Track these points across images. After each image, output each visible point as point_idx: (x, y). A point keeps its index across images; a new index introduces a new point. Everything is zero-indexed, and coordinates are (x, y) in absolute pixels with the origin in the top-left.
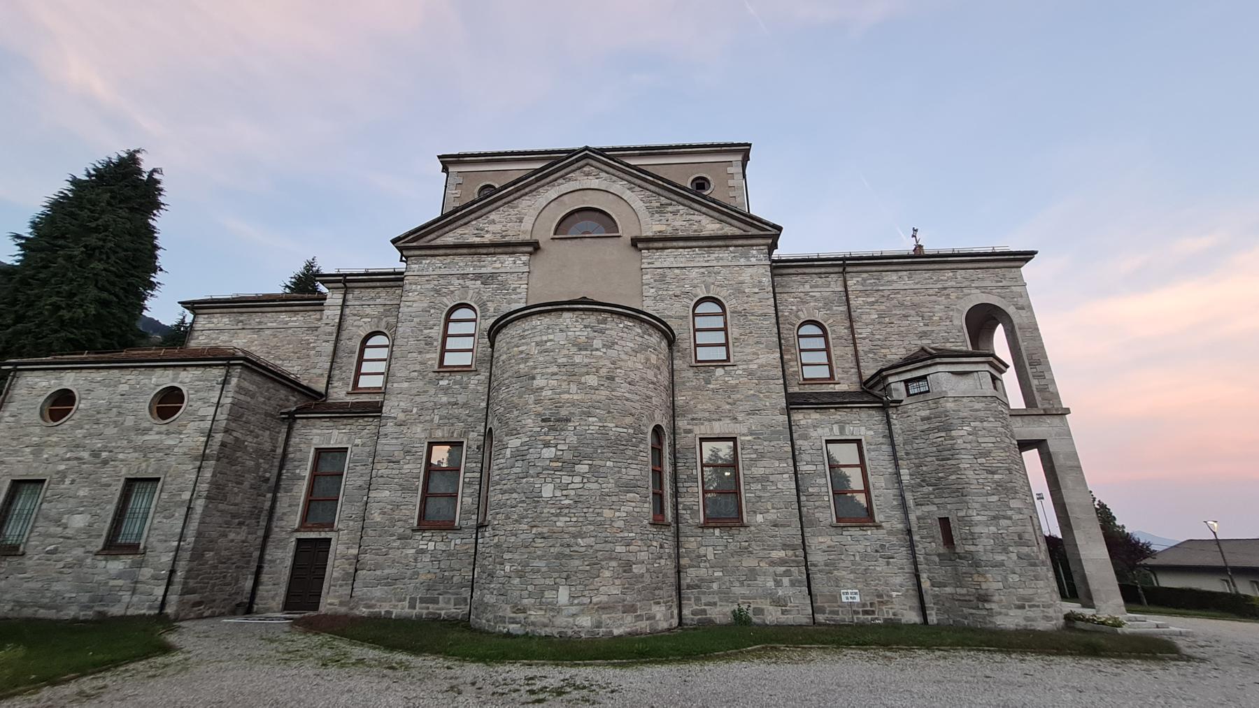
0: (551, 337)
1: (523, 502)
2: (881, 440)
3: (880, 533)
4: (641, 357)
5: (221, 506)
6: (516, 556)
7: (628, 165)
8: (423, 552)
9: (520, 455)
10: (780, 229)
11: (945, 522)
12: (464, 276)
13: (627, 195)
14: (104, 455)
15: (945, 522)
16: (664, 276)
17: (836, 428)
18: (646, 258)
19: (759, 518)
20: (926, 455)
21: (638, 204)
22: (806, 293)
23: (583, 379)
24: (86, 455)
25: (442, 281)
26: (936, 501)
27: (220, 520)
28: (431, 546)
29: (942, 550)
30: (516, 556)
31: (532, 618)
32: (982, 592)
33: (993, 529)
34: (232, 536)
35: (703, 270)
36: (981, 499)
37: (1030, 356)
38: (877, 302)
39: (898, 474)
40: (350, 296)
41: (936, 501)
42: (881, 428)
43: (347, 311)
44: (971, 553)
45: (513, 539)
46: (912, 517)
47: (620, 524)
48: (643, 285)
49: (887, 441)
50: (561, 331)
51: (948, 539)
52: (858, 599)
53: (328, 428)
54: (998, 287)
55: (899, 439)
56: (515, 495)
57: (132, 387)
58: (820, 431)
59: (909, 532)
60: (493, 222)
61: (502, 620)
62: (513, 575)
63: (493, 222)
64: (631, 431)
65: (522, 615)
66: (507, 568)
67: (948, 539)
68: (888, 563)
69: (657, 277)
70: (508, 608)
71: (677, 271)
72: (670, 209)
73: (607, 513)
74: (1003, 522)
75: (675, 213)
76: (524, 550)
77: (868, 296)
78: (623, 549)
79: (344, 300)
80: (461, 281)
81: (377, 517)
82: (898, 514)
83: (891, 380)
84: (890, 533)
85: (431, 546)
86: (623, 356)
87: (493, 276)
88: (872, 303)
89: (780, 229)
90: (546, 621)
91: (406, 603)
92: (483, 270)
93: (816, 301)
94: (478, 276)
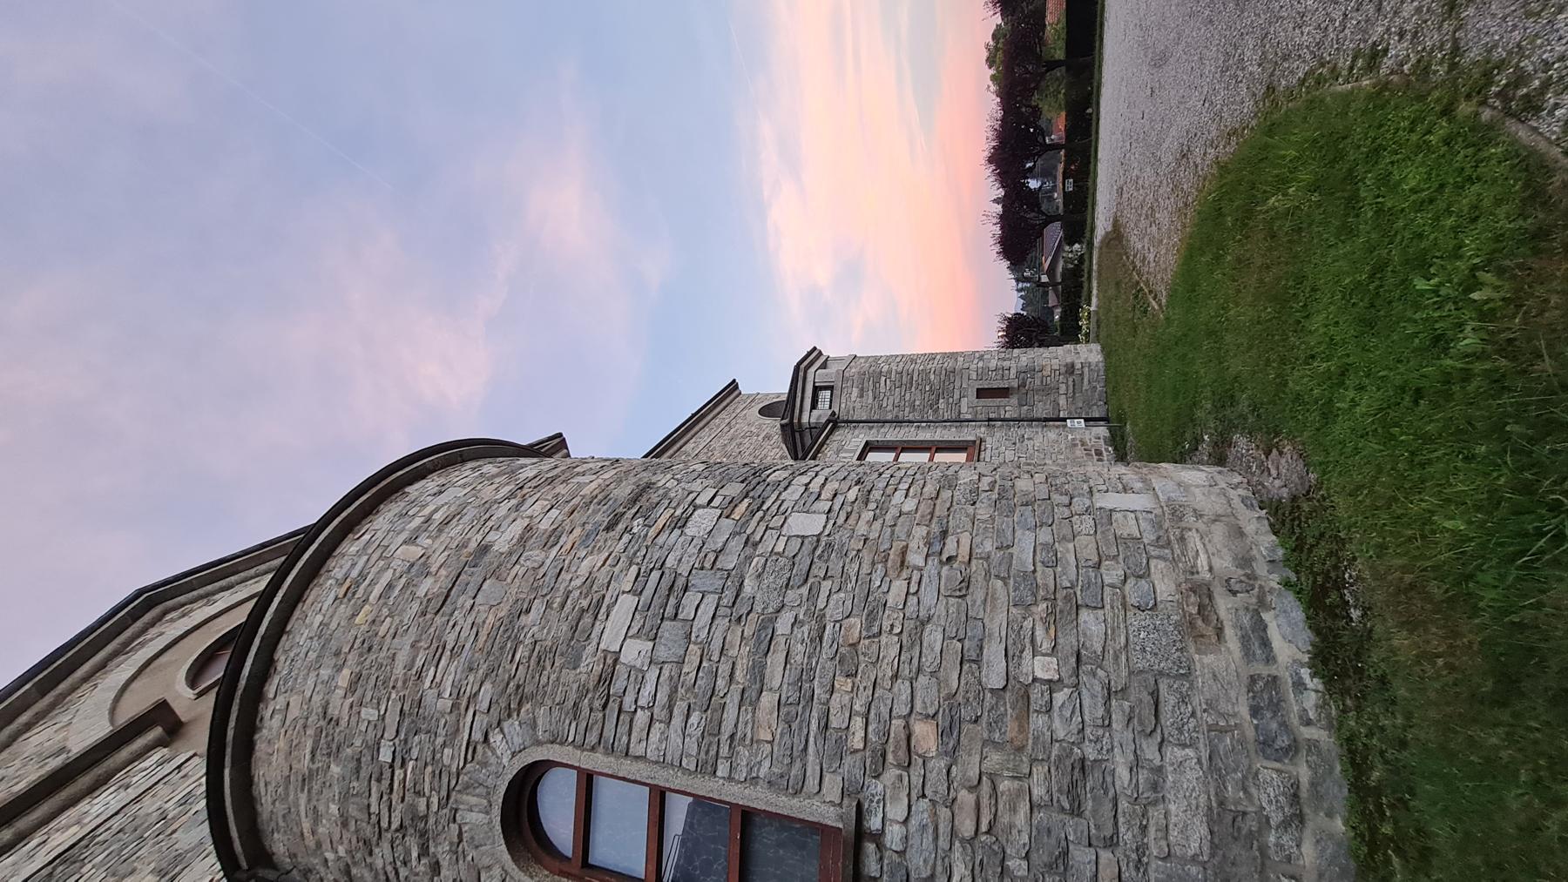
1: (813, 595)
6: (997, 622)
7: (266, 573)
9: (663, 603)
10: (560, 435)
11: (981, 393)
15: (981, 393)
20: (902, 397)
26: (956, 396)
29: (1014, 400)
30: (997, 622)
31: (1224, 563)
32: (1063, 370)
41: (956, 396)
44: (1019, 373)
45: (933, 636)
51: (1004, 393)
56: (783, 625)
61: (1266, 695)
62: (1068, 642)
65: (1224, 605)
66: (1043, 668)
67: (1004, 393)
70: (1206, 662)
76: (977, 594)
83: (805, 419)
89: (560, 435)
90: (1219, 531)
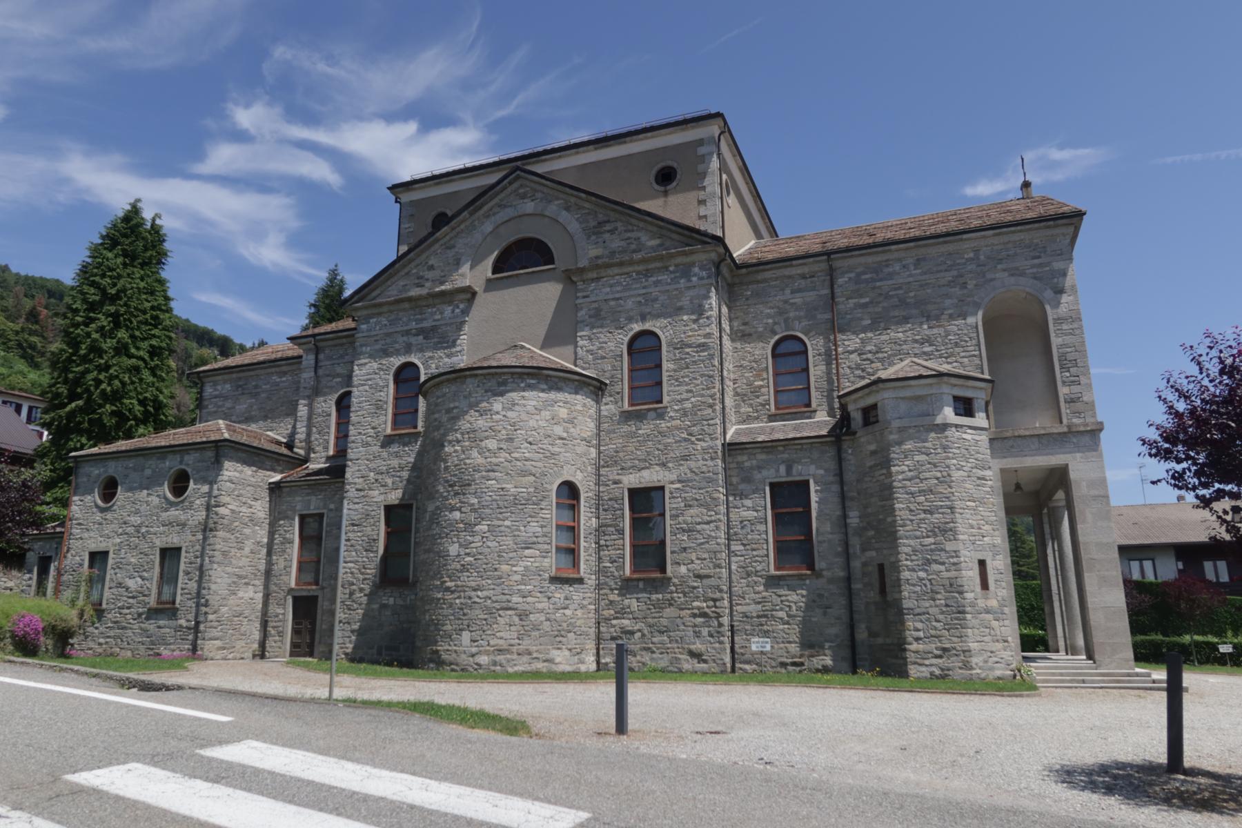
0: (457, 404)
2: (831, 478)
3: (821, 583)
4: (546, 414)
5: (229, 569)
8: (384, 606)
12: (407, 333)
13: (564, 216)
14: (144, 530)
16: (598, 310)
17: (783, 469)
18: (582, 290)
19: (683, 569)
21: (574, 226)
22: (786, 302)
23: (483, 444)
24: (130, 530)
25: (388, 340)
27: (229, 581)
28: (391, 601)
33: (922, 574)
34: (241, 594)
35: (639, 299)
36: (912, 542)
37: (1062, 357)
38: (871, 302)
39: (845, 516)
40: (321, 356)
42: (832, 465)
43: (321, 372)
46: (856, 564)
47: (517, 577)
48: (578, 322)
49: (838, 478)
50: (465, 397)
52: (768, 648)
53: (308, 494)
54: (1033, 266)
55: (849, 476)
57: (154, 471)
58: (765, 473)
59: (849, 579)
60: (431, 268)
63: (431, 268)
64: (532, 490)
68: (825, 614)
69: (592, 312)
71: (612, 303)
72: (608, 227)
73: (505, 568)
74: (935, 567)
75: (612, 232)
77: (861, 296)
78: (520, 600)
79: (317, 359)
80: (405, 338)
81: (725, 596)
82: (840, 560)
84: (830, 581)
85: (391, 601)
86: (524, 416)
87: (434, 329)
88: (865, 306)
91: (375, 651)
92: (425, 324)
93: (796, 310)
94: (420, 332)
